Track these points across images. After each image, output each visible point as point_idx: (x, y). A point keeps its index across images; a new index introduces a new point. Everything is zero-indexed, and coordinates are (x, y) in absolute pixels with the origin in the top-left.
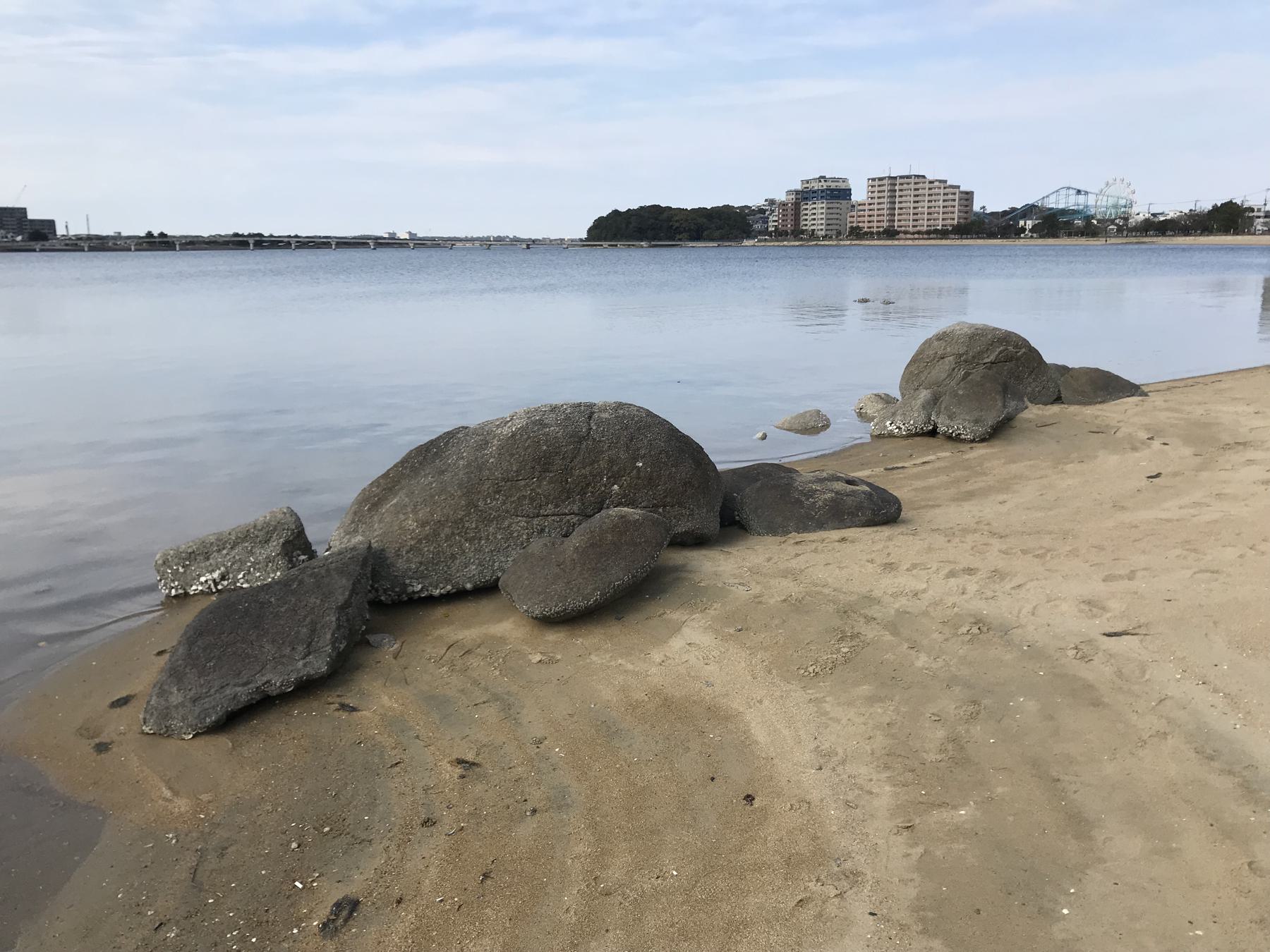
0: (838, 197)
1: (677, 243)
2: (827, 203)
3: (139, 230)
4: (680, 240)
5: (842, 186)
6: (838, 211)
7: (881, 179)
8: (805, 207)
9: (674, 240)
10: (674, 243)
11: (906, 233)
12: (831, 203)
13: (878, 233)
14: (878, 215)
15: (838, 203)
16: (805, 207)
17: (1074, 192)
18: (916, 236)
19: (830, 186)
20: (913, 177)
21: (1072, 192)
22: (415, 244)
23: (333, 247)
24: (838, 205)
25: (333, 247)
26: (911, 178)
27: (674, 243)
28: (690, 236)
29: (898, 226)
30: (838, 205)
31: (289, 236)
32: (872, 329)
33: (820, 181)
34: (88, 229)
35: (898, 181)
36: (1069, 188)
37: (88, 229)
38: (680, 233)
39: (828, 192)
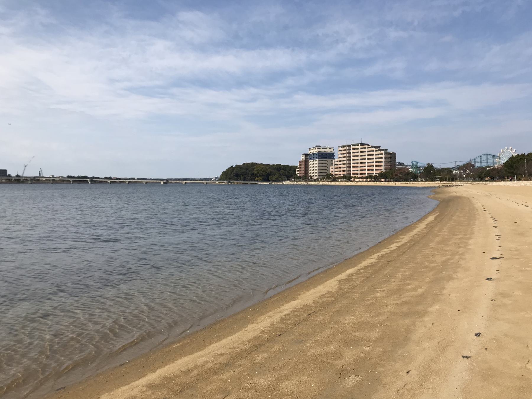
0: (325, 158)
1: (256, 182)
2: (319, 161)
3: (149, 178)
4: (257, 181)
5: (329, 151)
6: (326, 165)
7: (344, 147)
8: (310, 163)
9: (255, 181)
10: (255, 182)
11: (355, 178)
12: (321, 161)
13: (341, 178)
14: (368, 170)
15: (326, 161)
16: (310, 163)
17: (491, 156)
18: (360, 179)
19: (321, 151)
20: (359, 145)
21: (489, 156)
22: (111, 181)
23: (71, 182)
24: (326, 162)
25: (71, 182)
26: (358, 145)
27: (255, 182)
28: (262, 178)
29: (353, 174)
30: (326, 162)
31: (106, 178)
32: (3, 217)
33: (316, 149)
34: (23, 173)
35: (352, 147)
36: (487, 155)
37: (23, 173)
38: (258, 177)
39: (319, 155)
